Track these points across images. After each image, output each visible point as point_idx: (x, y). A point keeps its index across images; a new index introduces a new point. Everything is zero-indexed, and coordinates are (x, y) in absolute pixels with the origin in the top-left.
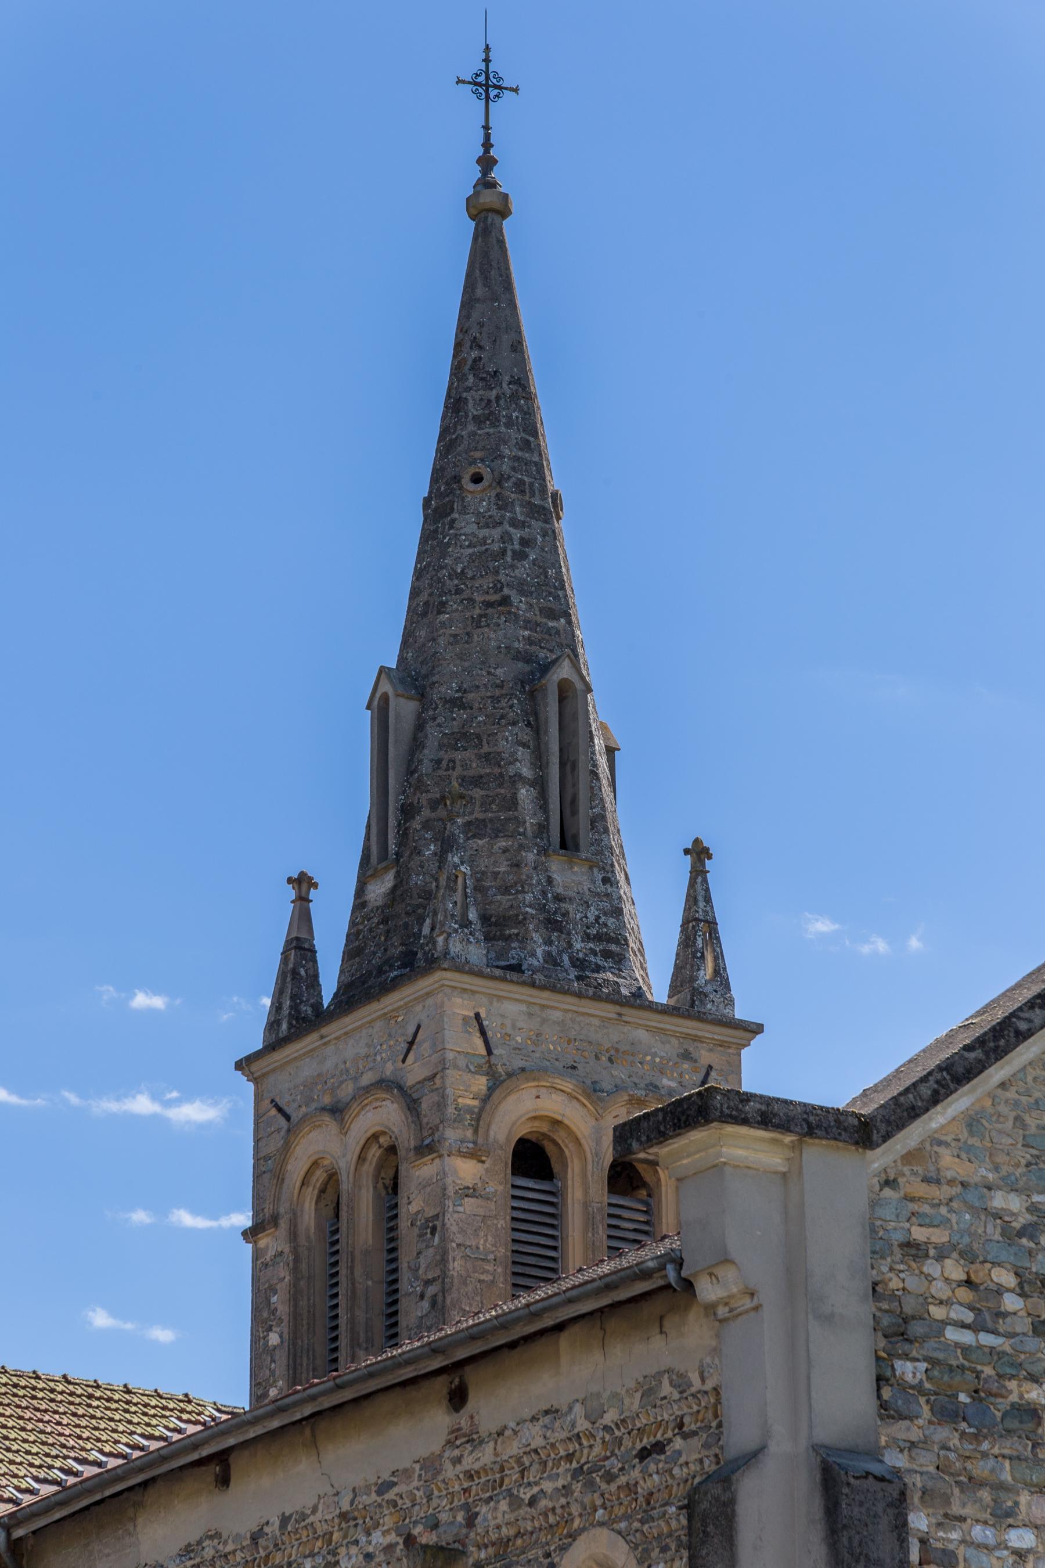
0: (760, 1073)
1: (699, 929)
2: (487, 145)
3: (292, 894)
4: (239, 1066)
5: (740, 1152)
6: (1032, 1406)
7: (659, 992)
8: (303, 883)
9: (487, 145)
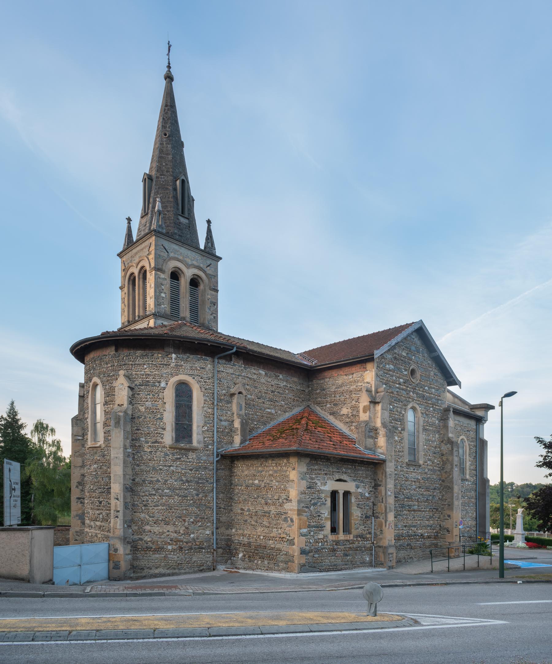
0: (232, 323)
1: (209, 231)
2: (169, 63)
3: (127, 222)
4: (118, 255)
5: (369, 570)
6: (483, 422)
7: (202, 247)
8: (129, 220)
9: (169, 63)
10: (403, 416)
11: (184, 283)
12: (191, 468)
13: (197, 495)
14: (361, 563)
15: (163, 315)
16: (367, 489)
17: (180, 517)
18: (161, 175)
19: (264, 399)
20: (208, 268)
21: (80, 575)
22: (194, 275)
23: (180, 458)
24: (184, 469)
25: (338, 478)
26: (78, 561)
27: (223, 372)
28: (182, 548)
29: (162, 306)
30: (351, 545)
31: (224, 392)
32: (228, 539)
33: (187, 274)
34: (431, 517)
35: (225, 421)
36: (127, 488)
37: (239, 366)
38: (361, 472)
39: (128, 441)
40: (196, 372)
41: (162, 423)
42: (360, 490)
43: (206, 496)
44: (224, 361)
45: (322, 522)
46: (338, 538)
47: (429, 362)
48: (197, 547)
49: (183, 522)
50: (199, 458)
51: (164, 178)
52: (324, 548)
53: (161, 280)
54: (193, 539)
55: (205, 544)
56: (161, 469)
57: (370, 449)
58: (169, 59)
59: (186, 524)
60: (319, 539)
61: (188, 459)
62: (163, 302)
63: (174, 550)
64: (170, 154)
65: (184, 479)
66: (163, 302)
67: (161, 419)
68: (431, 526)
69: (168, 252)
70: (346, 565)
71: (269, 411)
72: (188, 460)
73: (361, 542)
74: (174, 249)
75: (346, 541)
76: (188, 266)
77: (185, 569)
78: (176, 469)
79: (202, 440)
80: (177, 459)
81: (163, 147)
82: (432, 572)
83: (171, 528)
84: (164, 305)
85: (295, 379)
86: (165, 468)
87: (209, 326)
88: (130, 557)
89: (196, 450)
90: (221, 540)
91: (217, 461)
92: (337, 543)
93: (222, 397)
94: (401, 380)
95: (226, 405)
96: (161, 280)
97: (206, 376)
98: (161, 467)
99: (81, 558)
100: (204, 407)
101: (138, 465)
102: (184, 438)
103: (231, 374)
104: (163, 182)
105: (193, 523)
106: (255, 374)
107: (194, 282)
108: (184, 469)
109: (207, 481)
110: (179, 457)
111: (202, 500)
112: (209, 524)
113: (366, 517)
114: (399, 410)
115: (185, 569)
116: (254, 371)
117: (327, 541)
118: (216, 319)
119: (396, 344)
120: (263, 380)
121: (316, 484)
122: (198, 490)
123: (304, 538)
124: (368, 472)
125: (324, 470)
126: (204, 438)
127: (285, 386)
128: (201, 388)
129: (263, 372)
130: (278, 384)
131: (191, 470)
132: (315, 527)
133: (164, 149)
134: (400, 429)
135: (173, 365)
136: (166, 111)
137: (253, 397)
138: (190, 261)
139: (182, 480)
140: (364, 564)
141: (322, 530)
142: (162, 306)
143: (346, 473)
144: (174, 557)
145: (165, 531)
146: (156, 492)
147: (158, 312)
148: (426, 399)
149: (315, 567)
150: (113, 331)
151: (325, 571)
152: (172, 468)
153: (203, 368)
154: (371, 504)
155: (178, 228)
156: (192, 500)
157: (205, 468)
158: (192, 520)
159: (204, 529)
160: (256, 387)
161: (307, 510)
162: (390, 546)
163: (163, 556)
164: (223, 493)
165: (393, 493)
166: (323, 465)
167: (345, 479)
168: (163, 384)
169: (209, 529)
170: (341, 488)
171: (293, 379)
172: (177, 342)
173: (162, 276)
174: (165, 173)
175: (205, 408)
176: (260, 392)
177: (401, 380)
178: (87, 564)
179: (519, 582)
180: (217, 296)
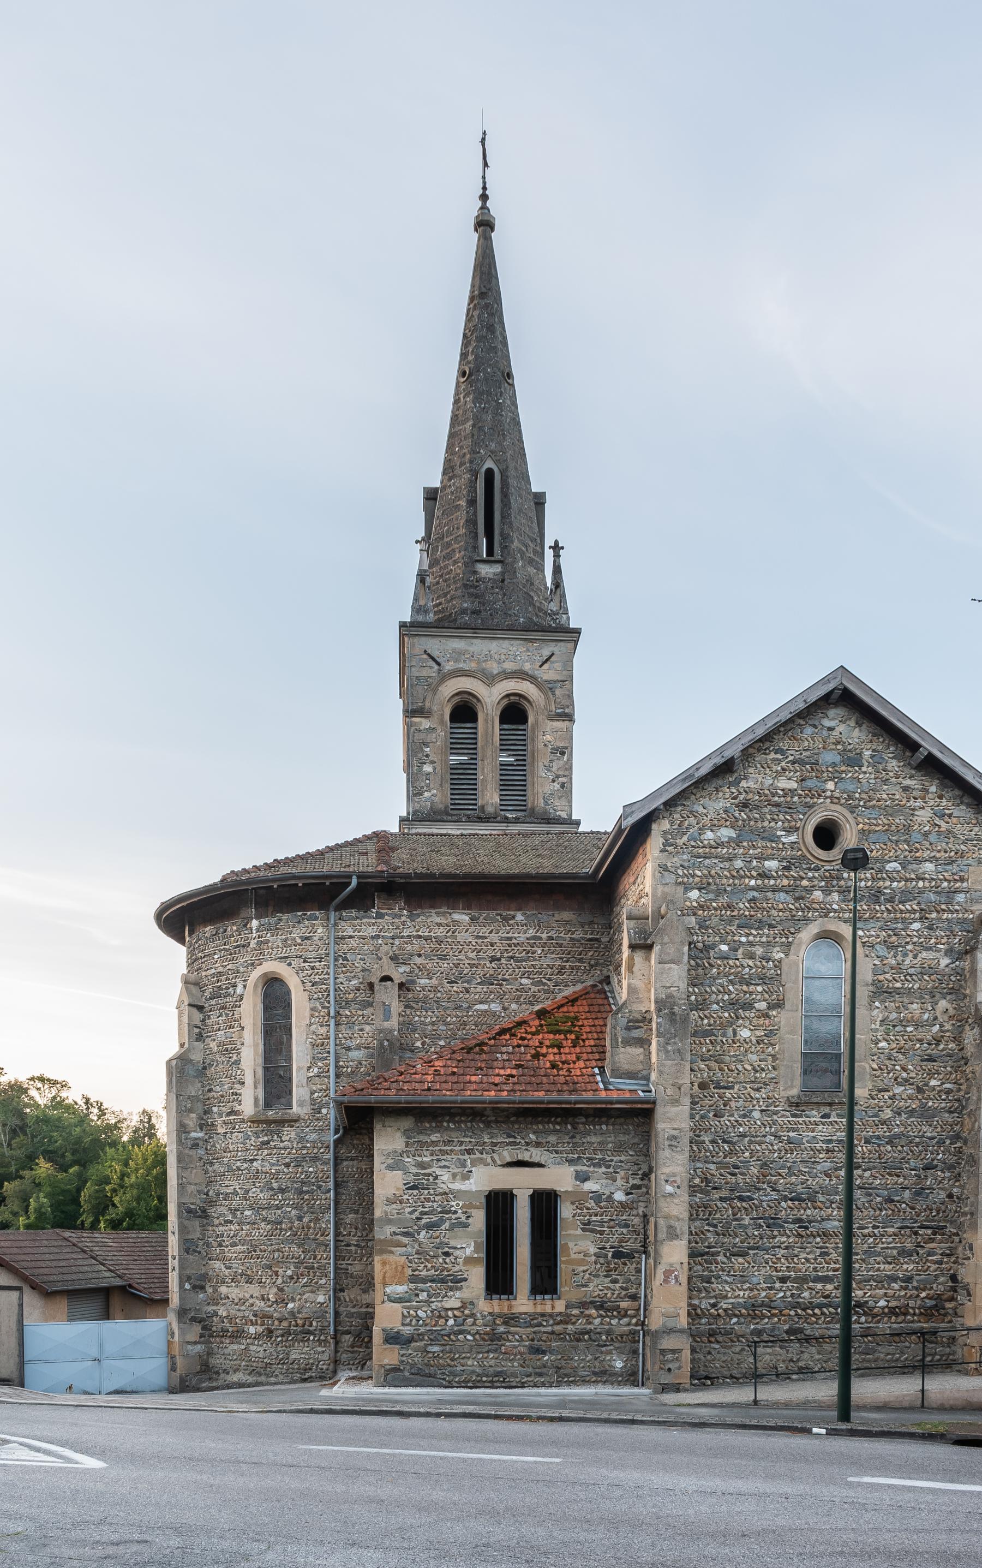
2: (485, 188)
9: (485, 188)
10: (778, 964)
11: (489, 723)
12: (287, 1160)
13: (300, 1218)
14: (595, 1373)
15: (428, 814)
16: (619, 1182)
17: (270, 1267)
19: (468, 982)
20: (546, 666)
21: (100, 1378)
22: (508, 696)
23: (268, 1142)
24: (274, 1165)
25: (509, 1159)
26: (95, 1353)
27: (351, 937)
28: (270, 1331)
29: (426, 794)
30: (558, 1328)
31: (354, 982)
32: (367, 1313)
33: (488, 701)
34: (904, 1253)
35: (358, 1048)
36: (189, 1211)
37: (395, 916)
38: (594, 1139)
39: (193, 1115)
40: (293, 951)
41: (239, 1072)
42: (589, 1186)
43: (317, 1219)
44: (354, 913)
45: (457, 1268)
46: (510, 1307)
47: (908, 782)
48: (299, 1329)
49: (274, 1277)
50: (301, 1139)
52: (461, 1332)
53: (422, 736)
54: (292, 1313)
55: (314, 1324)
56: (238, 1169)
57: (631, 1075)
59: (280, 1281)
60: (447, 1309)
61: (282, 1141)
62: (428, 785)
63: (258, 1337)
65: (275, 1185)
66: (428, 785)
67: (237, 1062)
68: (908, 1279)
69: (439, 664)
70: (540, 1375)
71: (484, 1007)
72: (282, 1145)
73: (597, 1321)
74: (454, 650)
75: (543, 1315)
76: (490, 680)
77: (277, 1376)
78: (262, 1166)
79: (307, 1098)
80: (263, 1143)
82: (923, 1406)
83: (254, 1290)
84: (429, 790)
85: (566, 915)
86: (245, 1165)
87: (546, 812)
88: (199, 1348)
89: (296, 1121)
90: (350, 1315)
91: (337, 1142)
92: (511, 1319)
93: (351, 996)
94: (772, 865)
95: (360, 1013)
96: (422, 736)
97: (313, 955)
98: (239, 1164)
99: (101, 1346)
100: (310, 1024)
101: (212, 1164)
102: (279, 1097)
103: (373, 938)
105: (291, 1278)
106: (439, 925)
107: (514, 713)
108: (274, 1165)
109: (319, 1187)
110: (266, 1139)
111: (309, 1228)
112: (323, 1281)
113: (618, 1255)
114: (759, 951)
115: (277, 1376)
116: (438, 920)
117: (472, 1315)
118: (566, 789)
120: (463, 937)
121: (436, 1178)
122: (301, 1209)
123: (397, 1306)
124: (622, 1138)
125: (461, 1143)
126: (312, 1094)
127: (534, 938)
128: (303, 983)
129: (462, 917)
130: (508, 939)
131: (287, 1165)
132: (433, 1281)
134: (762, 1006)
135: (253, 944)
137: (434, 981)
138: (495, 665)
139: (272, 1189)
140: (604, 1376)
141: (460, 1288)
142: (426, 794)
143: (538, 1145)
144: (259, 1350)
145: (247, 1296)
146: (234, 1216)
147: (415, 813)
148: (891, 900)
149: (430, 1376)
151: (463, 1385)
152: (255, 1164)
153: (307, 938)
154: (637, 1220)
155: (471, 595)
156: (291, 1229)
157: (315, 1159)
158: (289, 1273)
159: (312, 1292)
160: (443, 958)
161: (405, 1240)
162: (671, 1331)
163: (243, 1347)
164: (356, 1212)
165: (685, 1188)
166: (459, 1129)
167: (535, 1159)
168: (239, 990)
169: (322, 1291)
170: (522, 1184)
171: (557, 917)
172: (262, 892)
173: (425, 724)
175: (313, 1027)
176: (456, 966)
177: (772, 865)
178: (115, 1358)
179: (815, 1430)
180: (569, 732)
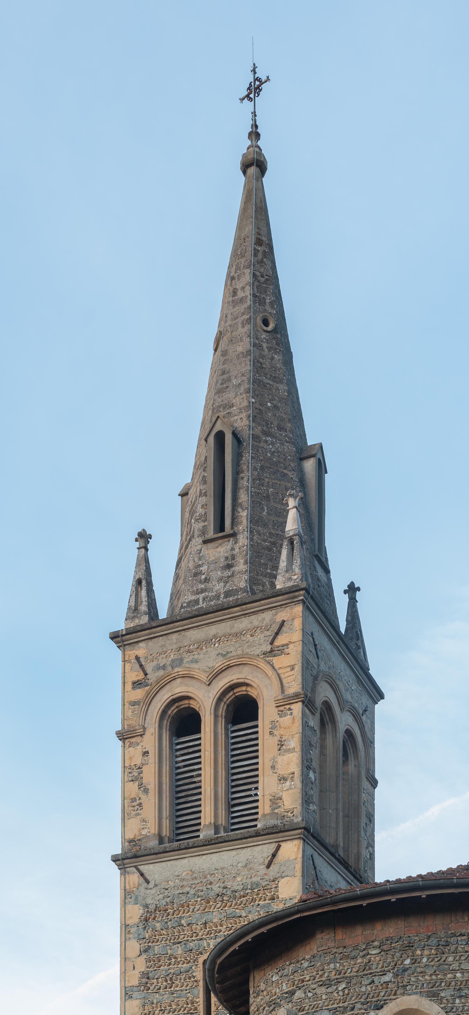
8: (144, 538)
18: (266, 434)
51: (273, 444)
58: (254, 114)
64: (281, 382)
81: (263, 357)
104: (272, 453)
119: (215, 636)
133: (267, 364)
136: (260, 256)
150: (420, 876)
174: (274, 430)
